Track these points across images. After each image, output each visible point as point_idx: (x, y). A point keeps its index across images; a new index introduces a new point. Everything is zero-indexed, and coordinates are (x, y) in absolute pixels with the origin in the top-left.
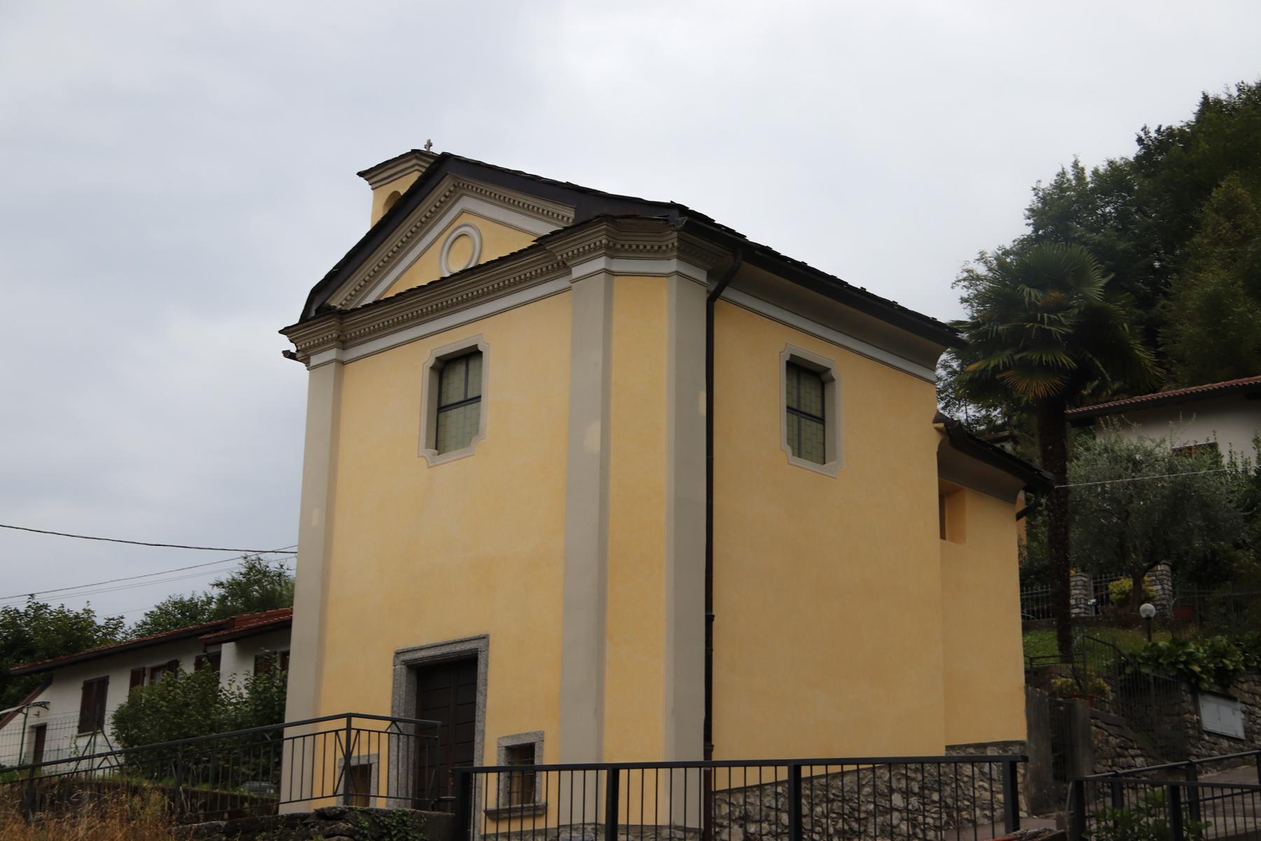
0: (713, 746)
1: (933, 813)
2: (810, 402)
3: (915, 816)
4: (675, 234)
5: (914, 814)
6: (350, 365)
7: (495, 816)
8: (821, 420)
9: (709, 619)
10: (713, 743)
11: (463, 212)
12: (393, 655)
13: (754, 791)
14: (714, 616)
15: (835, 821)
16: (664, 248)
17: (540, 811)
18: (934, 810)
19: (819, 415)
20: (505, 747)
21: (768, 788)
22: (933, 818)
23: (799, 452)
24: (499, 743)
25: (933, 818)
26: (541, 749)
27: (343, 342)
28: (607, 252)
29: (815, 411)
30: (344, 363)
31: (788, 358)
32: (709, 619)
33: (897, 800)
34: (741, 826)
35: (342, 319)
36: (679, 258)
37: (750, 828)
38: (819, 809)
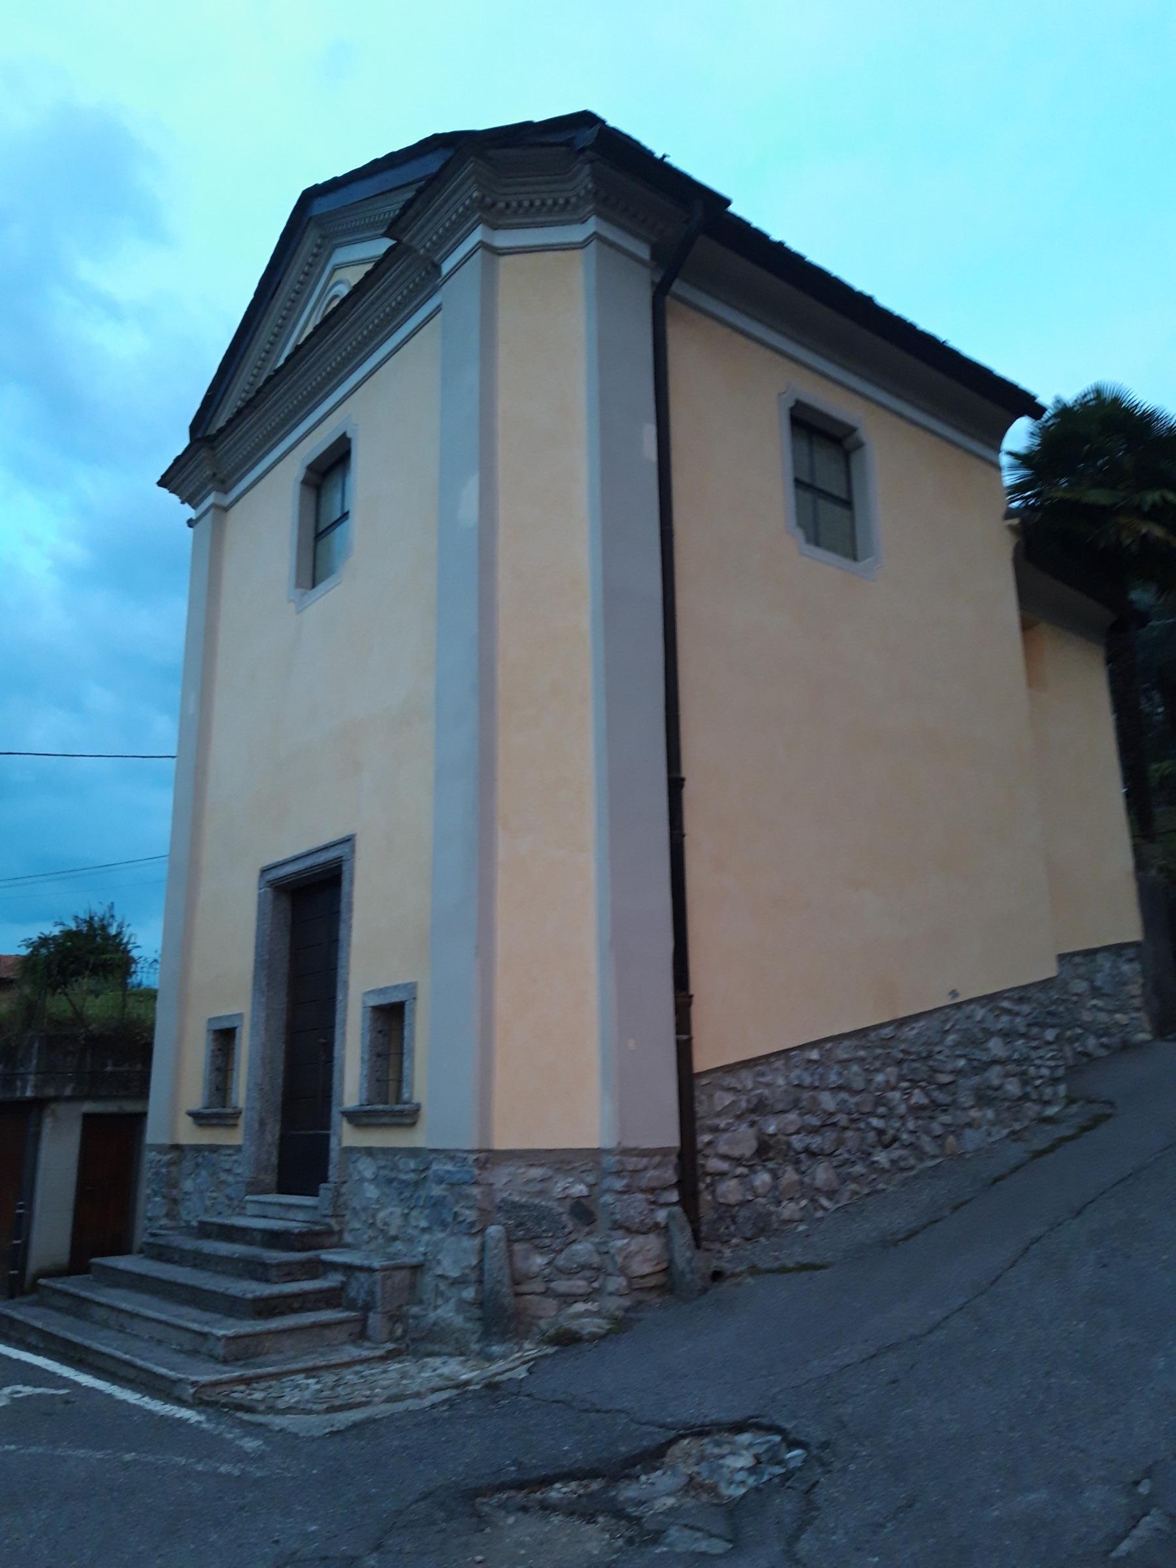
0: (691, 996)
1: (1049, 1059)
2: (828, 476)
3: (1024, 1068)
4: (587, 169)
5: (1022, 1065)
6: (232, 510)
7: (356, 1118)
8: (847, 504)
9: (675, 785)
10: (692, 992)
11: (334, 270)
12: (258, 873)
13: (770, 1063)
14: (683, 780)
15: (907, 1092)
16: (573, 200)
17: (408, 1117)
18: (1050, 1055)
19: (844, 496)
20: (373, 1007)
21: (795, 1056)
22: (1048, 1067)
23: (815, 538)
24: (364, 1002)
25: (1048, 1067)
26: (413, 1011)
27: (223, 482)
28: (485, 217)
29: (839, 491)
30: (226, 509)
31: (792, 404)
32: (675, 785)
33: (996, 1047)
34: (752, 1124)
35: (213, 449)
36: (599, 214)
37: (764, 1183)
38: (880, 1078)
